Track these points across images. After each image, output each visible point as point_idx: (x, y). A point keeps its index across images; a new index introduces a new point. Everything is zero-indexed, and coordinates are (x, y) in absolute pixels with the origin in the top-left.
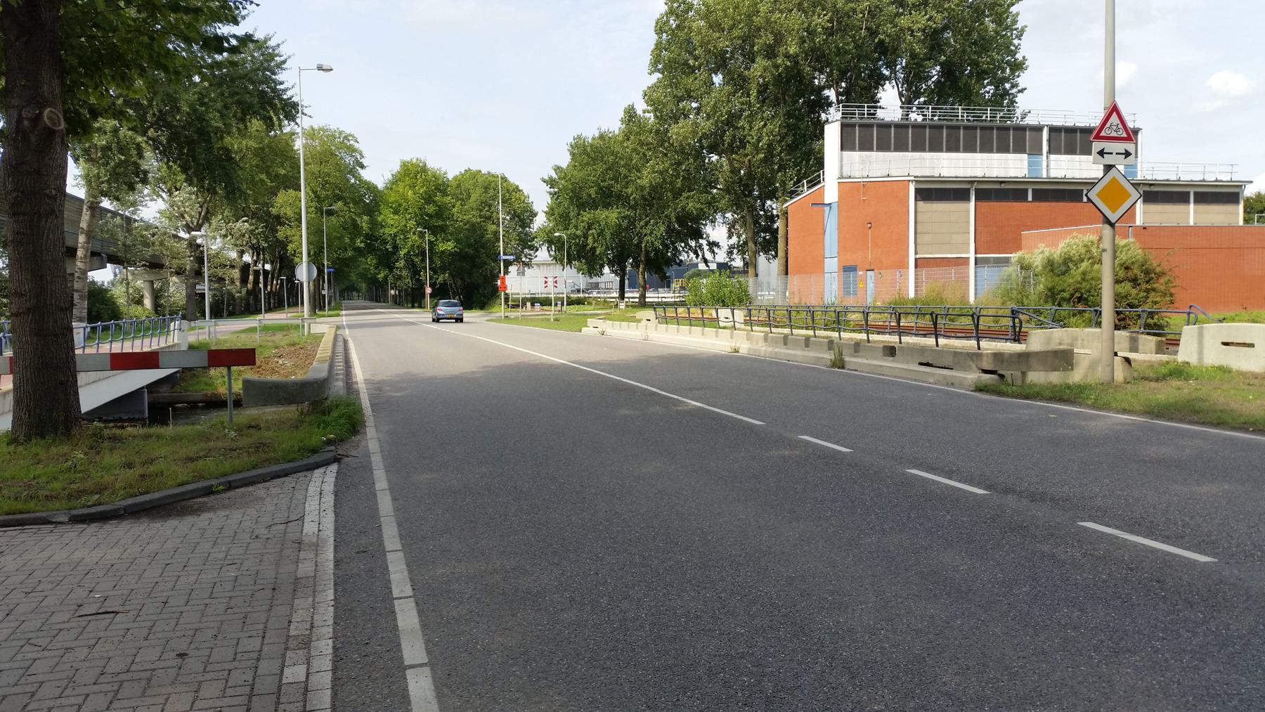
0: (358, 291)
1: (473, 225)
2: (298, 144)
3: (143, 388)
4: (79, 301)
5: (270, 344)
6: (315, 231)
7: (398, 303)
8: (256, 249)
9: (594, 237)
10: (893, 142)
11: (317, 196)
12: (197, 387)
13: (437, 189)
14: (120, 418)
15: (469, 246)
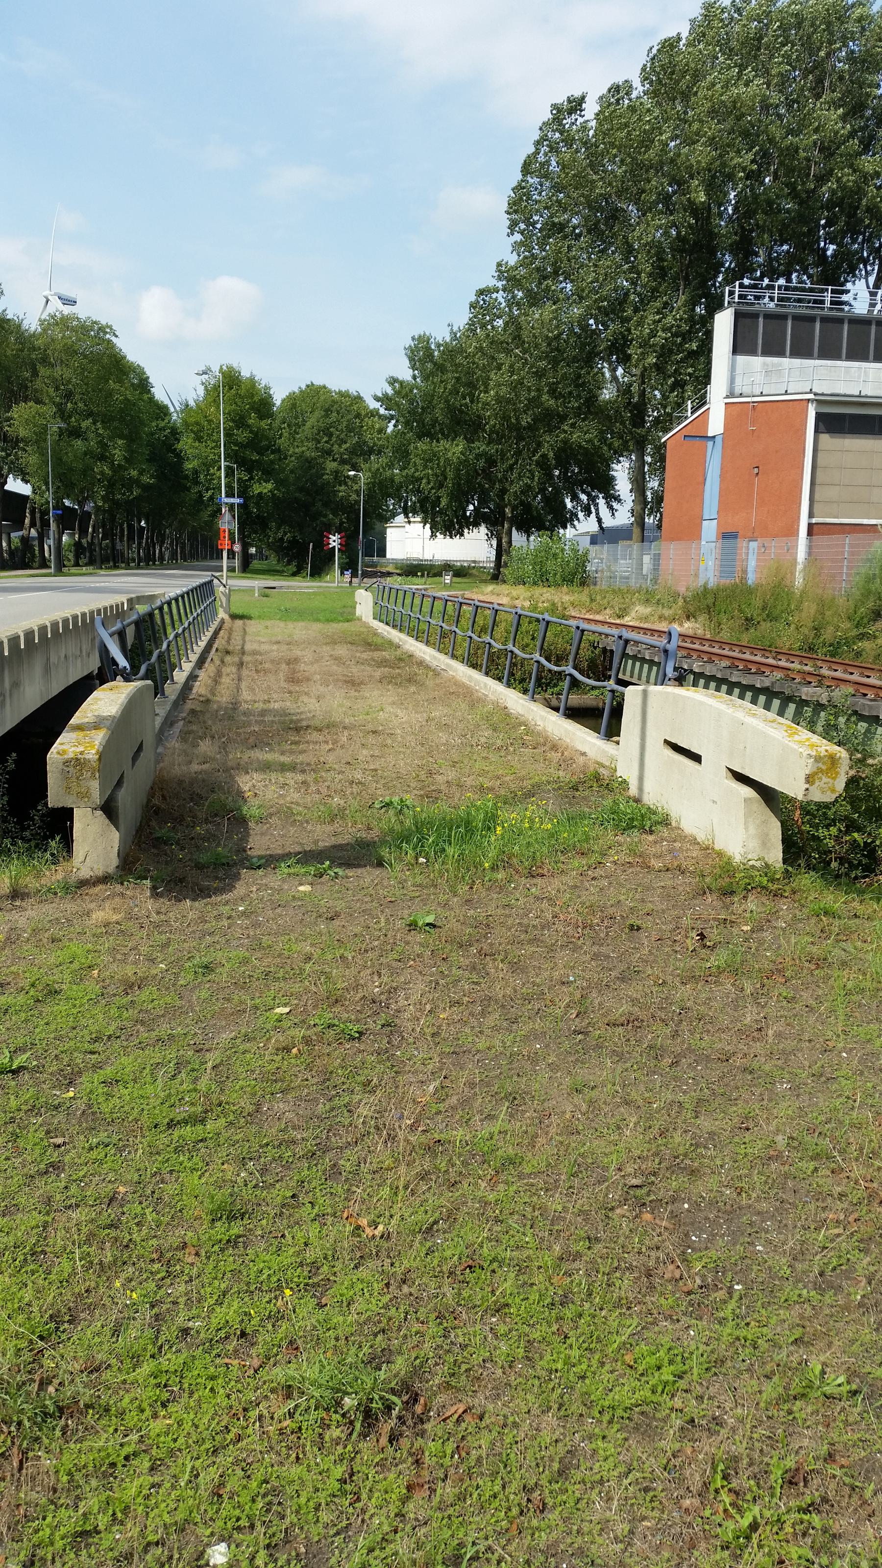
1: (308, 461)
10: (817, 344)
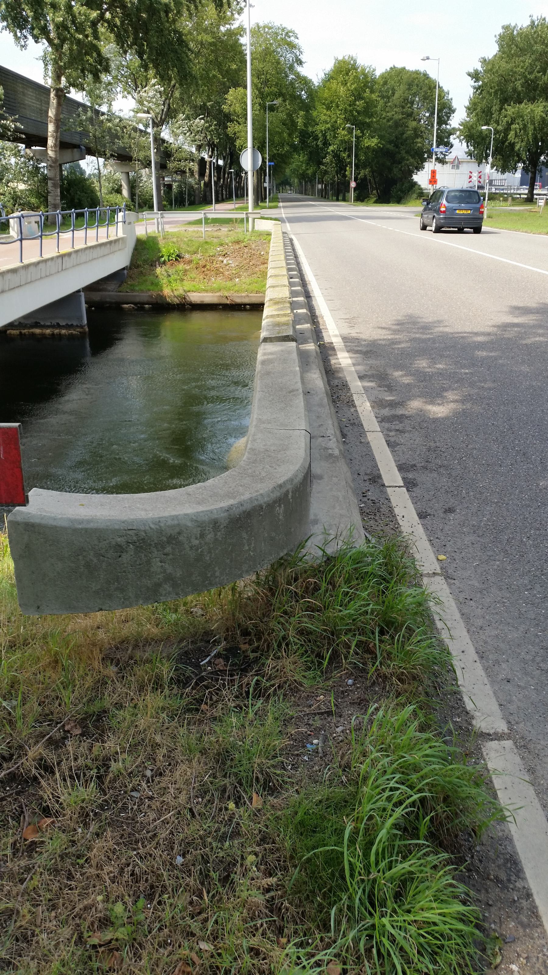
0: (290, 185)
2: (245, 40)
3: (78, 291)
4: (53, 189)
5: (215, 240)
6: (259, 126)
7: (324, 196)
8: (211, 145)
9: (516, 132)
11: (261, 93)
12: (143, 287)
13: (366, 86)
14: (58, 324)
15: (390, 142)
